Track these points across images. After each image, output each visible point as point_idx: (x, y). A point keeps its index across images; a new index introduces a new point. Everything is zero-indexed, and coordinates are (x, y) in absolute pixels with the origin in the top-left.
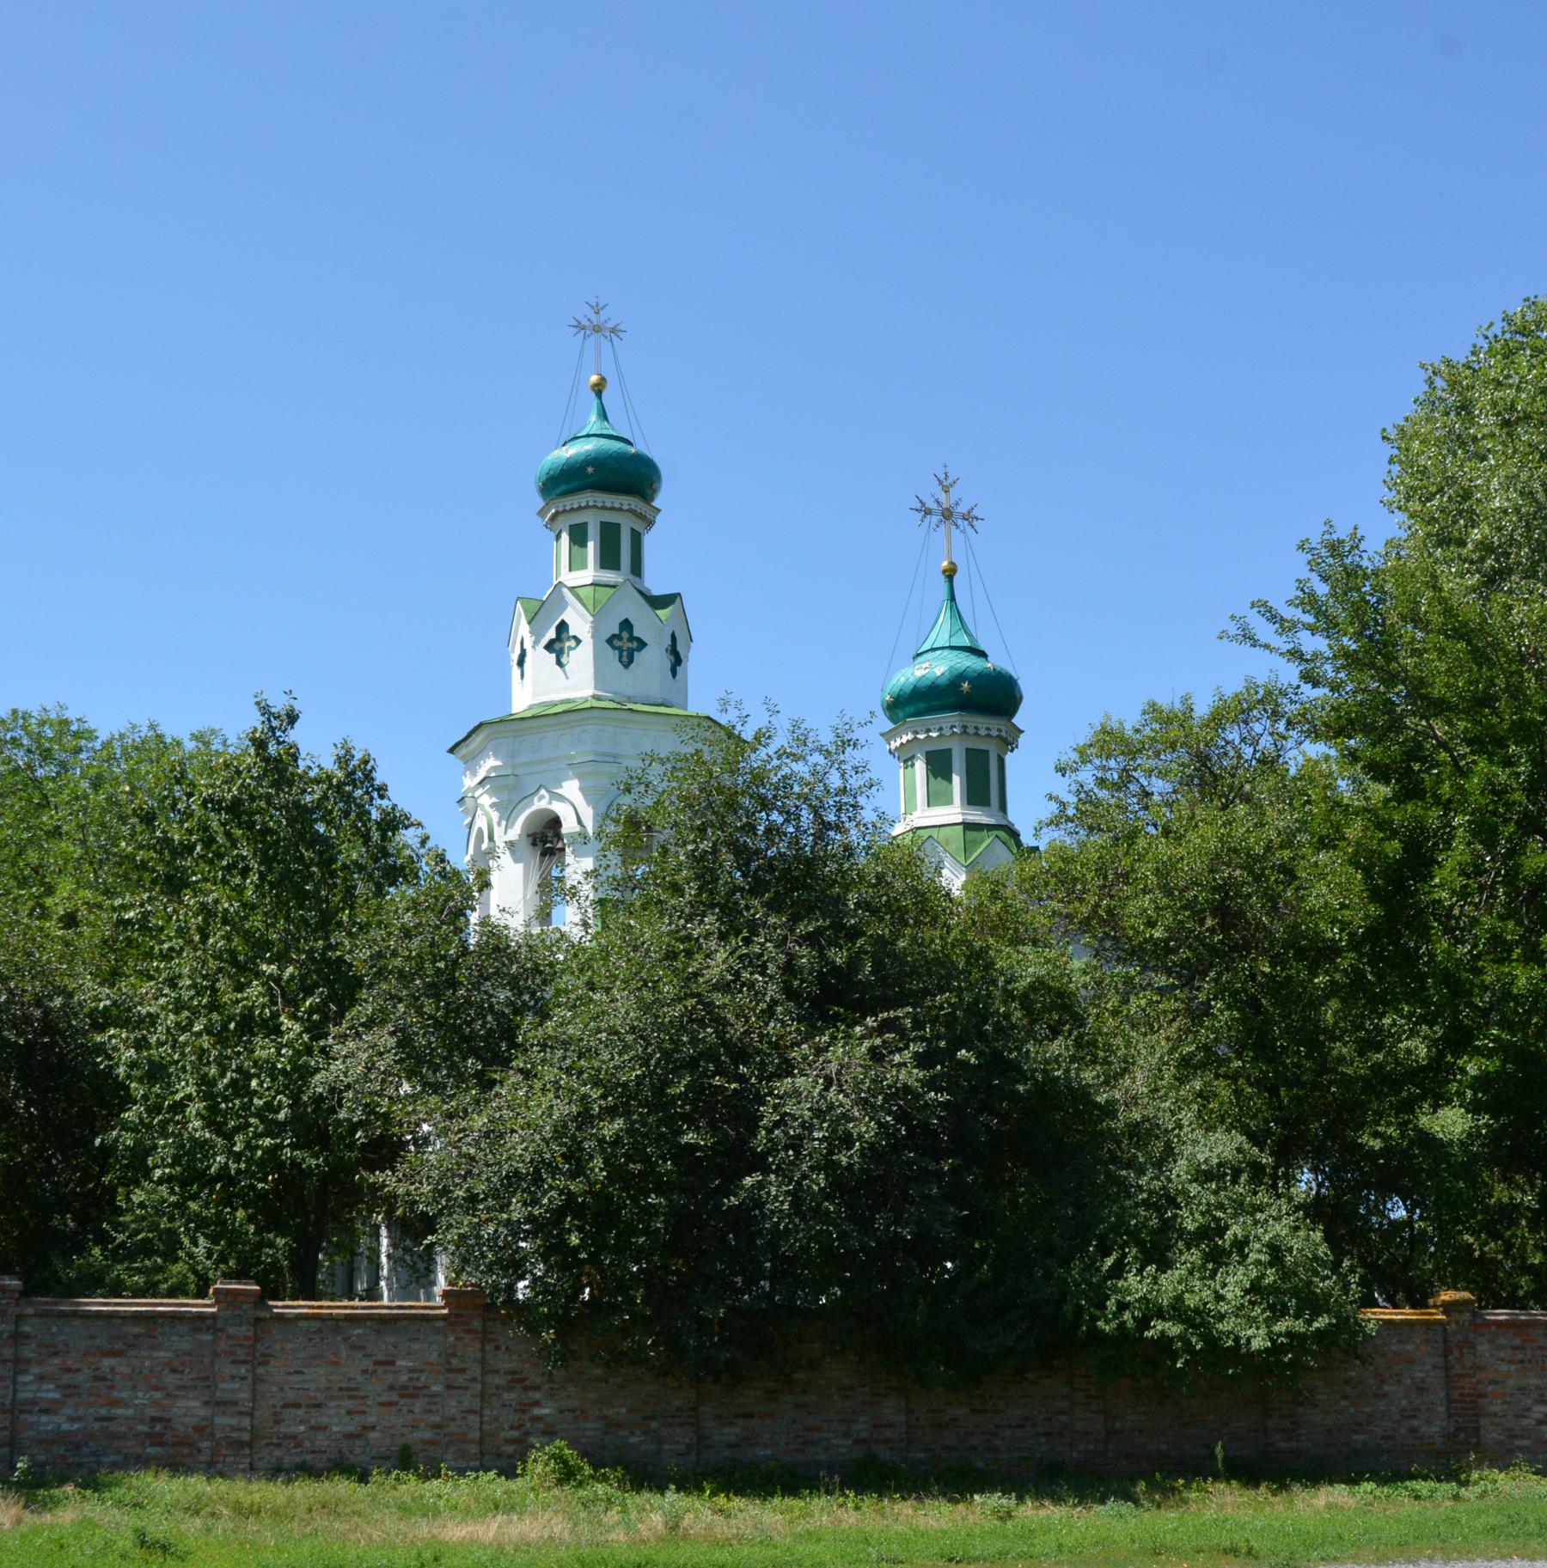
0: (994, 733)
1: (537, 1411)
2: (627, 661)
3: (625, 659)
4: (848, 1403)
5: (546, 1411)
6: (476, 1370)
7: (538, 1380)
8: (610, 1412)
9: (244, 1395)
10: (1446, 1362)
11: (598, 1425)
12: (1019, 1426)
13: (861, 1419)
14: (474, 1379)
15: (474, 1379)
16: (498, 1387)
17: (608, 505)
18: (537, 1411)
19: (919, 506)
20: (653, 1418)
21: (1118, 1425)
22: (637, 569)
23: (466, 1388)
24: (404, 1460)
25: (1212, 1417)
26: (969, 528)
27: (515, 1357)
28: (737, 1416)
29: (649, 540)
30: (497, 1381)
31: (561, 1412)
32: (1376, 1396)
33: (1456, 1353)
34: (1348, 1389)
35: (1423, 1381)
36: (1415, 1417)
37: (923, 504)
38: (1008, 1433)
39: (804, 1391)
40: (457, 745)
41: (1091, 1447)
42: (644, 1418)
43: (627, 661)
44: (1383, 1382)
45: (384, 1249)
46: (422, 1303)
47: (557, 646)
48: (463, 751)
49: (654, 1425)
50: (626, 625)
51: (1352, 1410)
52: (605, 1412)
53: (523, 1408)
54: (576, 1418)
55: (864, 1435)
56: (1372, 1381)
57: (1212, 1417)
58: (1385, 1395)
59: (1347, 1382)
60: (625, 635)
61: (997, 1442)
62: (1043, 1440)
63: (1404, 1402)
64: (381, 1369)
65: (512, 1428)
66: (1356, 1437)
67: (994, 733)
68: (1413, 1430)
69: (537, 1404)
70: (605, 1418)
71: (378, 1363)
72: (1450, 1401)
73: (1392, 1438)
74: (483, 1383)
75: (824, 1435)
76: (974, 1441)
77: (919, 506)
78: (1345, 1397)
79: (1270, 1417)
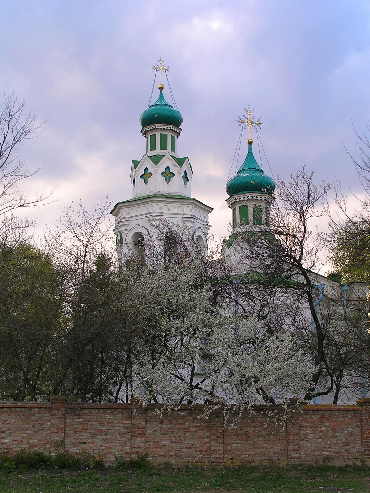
0: (263, 199)
1: (4, 441)
2: (168, 180)
3: (167, 180)
4: (123, 439)
5: (7, 441)
7: (4, 429)
8: (31, 441)
10: (361, 424)
11: (309, 437)
12: (189, 448)
13: (128, 445)
17: (163, 128)
18: (4, 441)
19: (239, 120)
20: (48, 444)
21: (229, 448)
22: (173, 149)
25: (266, 445)
26: (257, 127)
28: (79, 443)
29: (178, 140)
31: (13, 441)
32: (332, 437)
33: (365, 420)
34: (322, 434)
35: (352, 432)
36: (348, 445)
37: (241, 119)
38: (185, 450)
39: (106, 434)
41: (218, 456)
42: (44, 444)
43: (168, 180)
44: (336, 432)
46: (34, 402)
47: (144, 176)
48: (114, 213)
49: (48, 446)
50: (168, 168)
51: (323, 442)
52: (30, 441)
55: (129, 451)
56: (331, 432)
57: (266, 445)
58: (336, 437)
59: (321, 432)
60: (168, 172)
61: (181, 454)
62: (199, 453)
63: (344, 440)
66: (324, 453)
67: (263, 199)
68: (347, 450)
69: (4, 438)
70: (29, 443)
72: (362, 439)
73: (339, 453)
75: (113, 450)
76: (172, 453)
77: (239, 120)
78: (320, 438)
79: (289, 445)
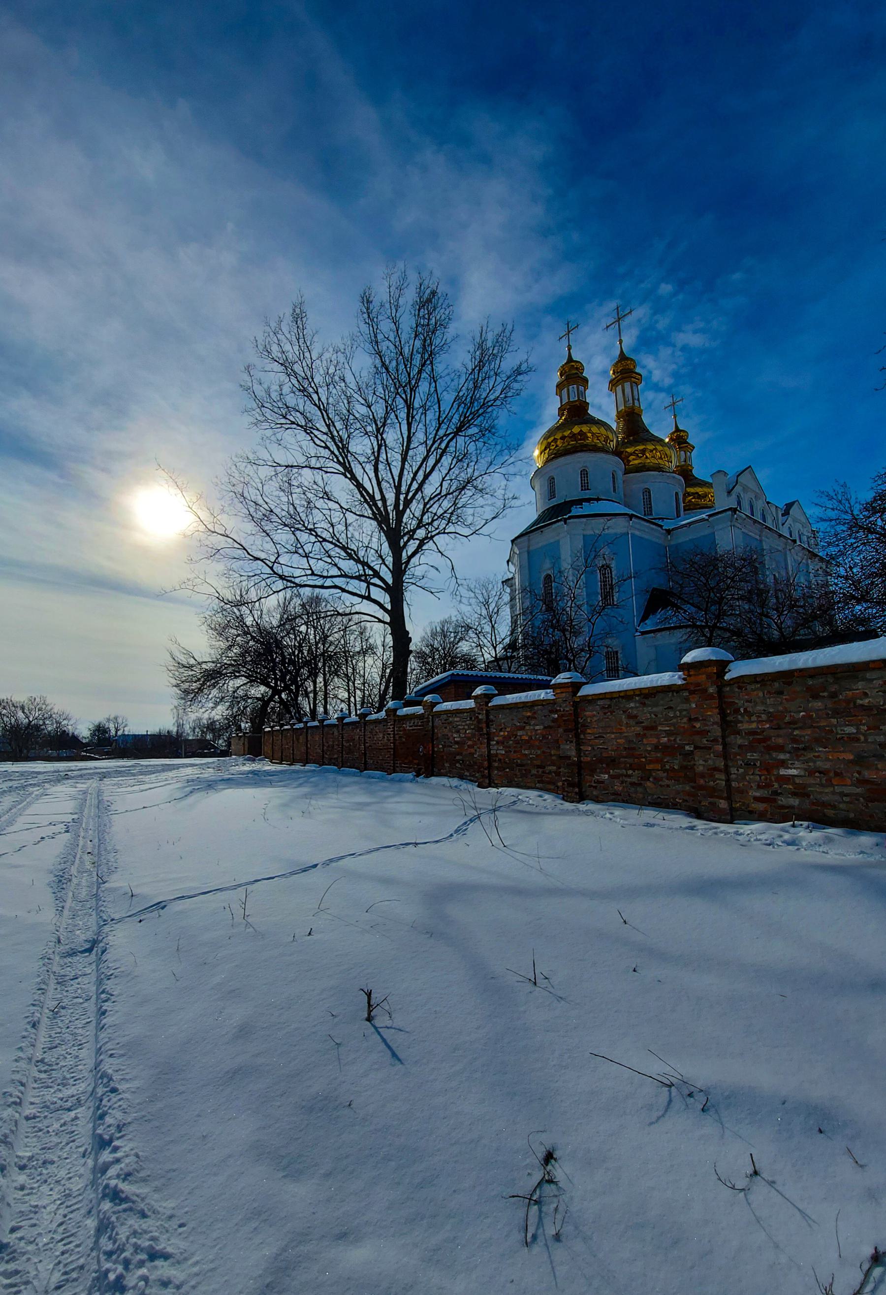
5: (794, 772)
6: (717, 731)
9: (573, 753)
14: (715, 740)
15: (715, 740)
16: (740, 747)
23: (710, 748)
24: (623, 801)
27: (754, 718)
30: (739, 741)
40: (331, 860)
45: (540, 677)
52: (866, 774)
53: (768, 768)
54: (829, 780)
64: (648, 733)
65: (759, 787)
69: (783, 764)
70: (866, 782)
71: (646, 728)
74: (725, 745)
